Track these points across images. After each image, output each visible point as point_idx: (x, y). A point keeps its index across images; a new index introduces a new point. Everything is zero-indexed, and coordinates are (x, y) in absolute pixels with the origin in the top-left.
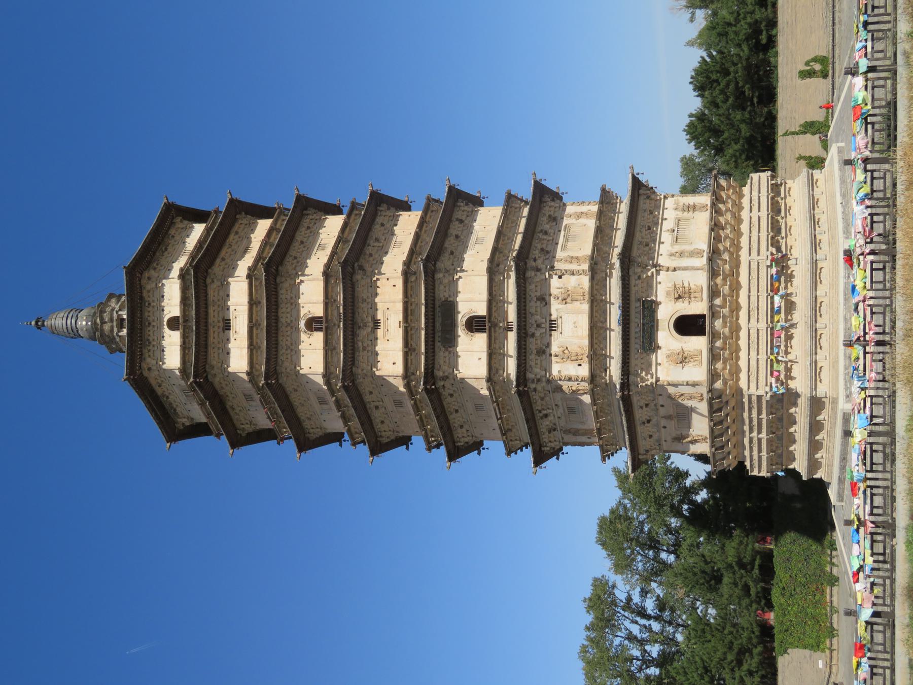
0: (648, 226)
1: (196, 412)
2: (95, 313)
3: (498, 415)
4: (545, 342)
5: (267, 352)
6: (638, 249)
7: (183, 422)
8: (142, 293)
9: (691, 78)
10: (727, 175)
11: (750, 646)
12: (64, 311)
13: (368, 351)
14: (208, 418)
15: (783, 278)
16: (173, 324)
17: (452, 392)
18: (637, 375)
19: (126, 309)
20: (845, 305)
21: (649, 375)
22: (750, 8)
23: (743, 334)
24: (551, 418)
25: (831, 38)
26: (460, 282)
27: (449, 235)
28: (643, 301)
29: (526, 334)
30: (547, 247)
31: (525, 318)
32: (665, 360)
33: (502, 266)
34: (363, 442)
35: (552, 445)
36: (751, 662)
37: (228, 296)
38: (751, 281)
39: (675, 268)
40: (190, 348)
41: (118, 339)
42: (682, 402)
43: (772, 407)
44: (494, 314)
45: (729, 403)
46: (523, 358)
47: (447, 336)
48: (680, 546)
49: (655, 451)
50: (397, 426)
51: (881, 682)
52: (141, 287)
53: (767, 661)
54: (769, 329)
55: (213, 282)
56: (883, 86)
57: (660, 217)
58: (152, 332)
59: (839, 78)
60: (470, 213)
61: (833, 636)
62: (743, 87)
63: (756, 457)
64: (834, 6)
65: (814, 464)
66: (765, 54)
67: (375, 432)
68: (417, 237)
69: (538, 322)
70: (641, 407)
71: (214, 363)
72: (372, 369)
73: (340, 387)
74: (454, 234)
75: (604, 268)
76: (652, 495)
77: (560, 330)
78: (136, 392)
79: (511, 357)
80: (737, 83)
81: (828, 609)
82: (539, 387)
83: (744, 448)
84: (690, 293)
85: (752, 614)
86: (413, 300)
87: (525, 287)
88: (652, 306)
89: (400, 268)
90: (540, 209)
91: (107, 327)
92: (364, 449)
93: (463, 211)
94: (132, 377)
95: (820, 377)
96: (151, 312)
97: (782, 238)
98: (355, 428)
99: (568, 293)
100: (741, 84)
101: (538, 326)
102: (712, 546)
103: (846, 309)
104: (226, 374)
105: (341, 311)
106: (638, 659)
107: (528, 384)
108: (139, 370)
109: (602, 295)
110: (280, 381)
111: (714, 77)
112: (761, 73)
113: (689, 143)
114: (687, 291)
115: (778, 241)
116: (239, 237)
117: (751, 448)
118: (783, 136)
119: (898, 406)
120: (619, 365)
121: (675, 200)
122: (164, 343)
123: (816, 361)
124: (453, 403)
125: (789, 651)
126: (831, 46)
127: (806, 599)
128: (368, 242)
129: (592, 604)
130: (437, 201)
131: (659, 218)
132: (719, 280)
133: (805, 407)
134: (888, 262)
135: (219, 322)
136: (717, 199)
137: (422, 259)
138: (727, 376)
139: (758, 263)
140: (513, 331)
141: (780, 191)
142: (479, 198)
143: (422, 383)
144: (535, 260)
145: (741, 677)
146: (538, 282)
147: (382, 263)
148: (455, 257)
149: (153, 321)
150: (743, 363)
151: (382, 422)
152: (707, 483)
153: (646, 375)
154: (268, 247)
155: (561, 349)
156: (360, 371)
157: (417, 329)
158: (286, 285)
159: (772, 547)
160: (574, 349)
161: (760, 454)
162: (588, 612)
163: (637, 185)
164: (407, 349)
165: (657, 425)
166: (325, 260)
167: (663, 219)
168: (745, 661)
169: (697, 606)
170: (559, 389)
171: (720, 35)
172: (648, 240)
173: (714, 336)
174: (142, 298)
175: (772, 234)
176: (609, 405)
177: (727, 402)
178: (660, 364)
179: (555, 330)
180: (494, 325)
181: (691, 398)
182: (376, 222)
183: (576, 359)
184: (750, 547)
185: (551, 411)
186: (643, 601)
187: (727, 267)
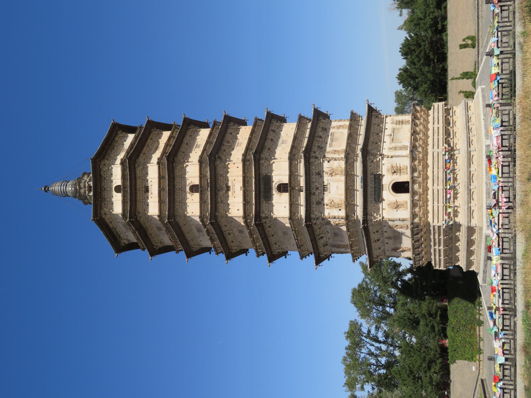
0: (377, 133)
1: (131, 236)
2: (76, 183)
3: (296, 237)
4: (321, 197)
5: (169, 204)
6: (372, 145)
7: (124, 242)
8: (100, 172)
9: (400, 49)
10: (420, 103)
11: (435, 359)
12: (59, 182)
13: (224, 203)
14: (137, 240)
15: (452, 161)
16: (118, 189)
17: (270, 225)
18: (372, 215)
19: (92, 181)
20: (486, 176)
21: (378, 215)
22: (432, 10)
23: (430, 192)
24: (324, 239)
25: (477, 26)
26: (274, 165)
27: (268, 139)
28: (375, 175)
29: (310, 193)
30: (321, 145)
31: (310, 184)
32: (387, 207)
33: (296, 156)
34: (222, 252)
35: (326, 253)
36: (436, 367)
37: (147, 174)
38: (434, 163)
39: (392, 156)
40: (127, 203)
41: (88, 197)
42: (397, 230)
43: (446, 232)
44: (293, 182)
45: (423, 230)
46: (309, 207)
47: (267, 195)
48: (396, 304)
49: (382, 256)
50: (241, 244)
51: (509, 397)
52: (100, 169)
53: (444, 367)
54: (444, 189)
55: (139, 166)
56: (508, 62)
57: (384, 127)
58: (106, 193)
59: (482, 48)
60: (279, 127)
61: (481, 353)
62: (429, 53)
63: (437, 259)
64: (478, 9)
65: (469, 263)
66: (440, 35)
67: (228, 247)
68: (250, 140)
69: (317, 187)
70: (374, 233)
71: (140, 210)
72: (226, 213)
73: (209, 223)
74: (270, 138)
75: (353, 157)
76: (381, 276)
77: (329, 191)
78: (98, 226)
79: (302, 206)
80: (425, 51)
81: (478, 339)
82: (318, 222)
83: (431, 254)
84: (400, 170)
85: (436, 342)
86: (248, 175)
87: (309, 168)
88: (379, 177)
89: (241, 157)
90: (317, 124)
91: (82, 191)
92: (222, 256)
93: (275, 125)
94: (96, 218)
95: (472, 216)
96: (106, 183)
97: (451, 139)
98: (217, 245)
99: (333, 170)
100: (427, 52)
101: (317, 189)
102: (414, 305)
103: (487, 178)
104: (147, 216)
105: (209, 182)
106: (374, 365)
107: (312, 221)
108: (100, 214)
109: (352, 171)
110: (176, 220)
111: (412, 48)
112: (439, 46)
113: (399, 84)
114: (399, 169)
115: (449, 141)
116: (153, 141)
117: (435, 255)
118: (451, 80)
119: (517, 244)
120: (362, 210)
121: (392, 118)
122: (113, 200)
123: (470, 207)
124: (271, 231)
125: (456, 361)
126: (477, 31)
127: (465, 333)
128: (223, 143)
129: (349, 335)
130: (261, 120)
131: (383, 128)
132: (416, 163)
133: (464, 232)
134: (511, 162)
135: (142, 188)
136: (415, 117)
137: (252, 153)
138: (421, 216)
139: (438, 153)
140: (303, 191)
141: (450, 113)
142: (284, 117)
143: (253, 221)
144: (315, 152)
145: (430, 375)
146: (316, 164)
147: (231, 155)
148: (270, 151)
149: (107, 188)
150: (430, 208)
151: (232, 242)
152: (410, 270)
153: (377, 215)
154: (168, 147)
155: (330, 201)
156: (219, 214)
157: (250, 191)
158: (179, 167)
159: (447, 304)
160: (337, 201)
161: (440, 258)
162: (347, 339)
163: (371, 110)
164: (245, 202)
165: (383, 242)
166: (199, 153)
167: (385, 129)
168: (432, 367)
169: (406, 336)
170: (329, 223)
171: (415, 25)
172: (377, 141)
173: (414, 193)
174: (100, 175)
175: (445, 137)
176: (357, 232)
177: (421, 230)
178: (384, 209)
179: (326, 191)
180: (292, 189)
181: (401, 227)
182: (227, 132)
183: (338, 207)
184: (435, 305)
185: (325, 235)
186: (377, 333)
187: (421, 155)
